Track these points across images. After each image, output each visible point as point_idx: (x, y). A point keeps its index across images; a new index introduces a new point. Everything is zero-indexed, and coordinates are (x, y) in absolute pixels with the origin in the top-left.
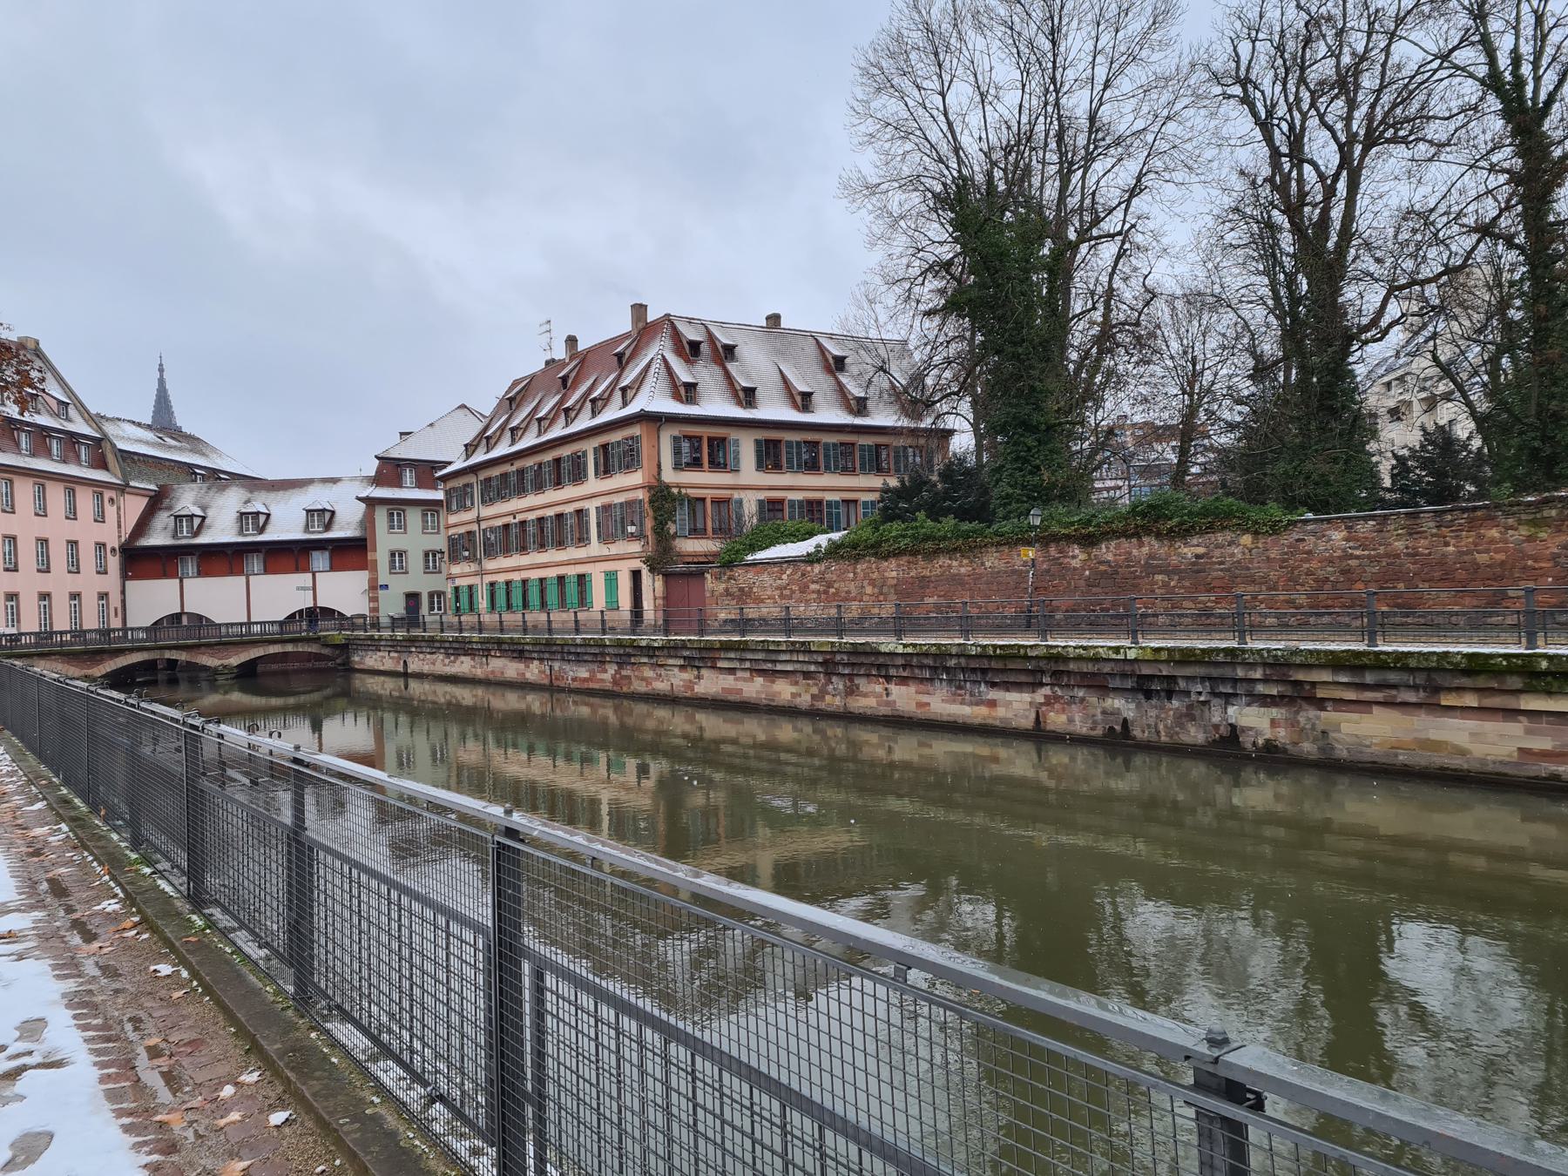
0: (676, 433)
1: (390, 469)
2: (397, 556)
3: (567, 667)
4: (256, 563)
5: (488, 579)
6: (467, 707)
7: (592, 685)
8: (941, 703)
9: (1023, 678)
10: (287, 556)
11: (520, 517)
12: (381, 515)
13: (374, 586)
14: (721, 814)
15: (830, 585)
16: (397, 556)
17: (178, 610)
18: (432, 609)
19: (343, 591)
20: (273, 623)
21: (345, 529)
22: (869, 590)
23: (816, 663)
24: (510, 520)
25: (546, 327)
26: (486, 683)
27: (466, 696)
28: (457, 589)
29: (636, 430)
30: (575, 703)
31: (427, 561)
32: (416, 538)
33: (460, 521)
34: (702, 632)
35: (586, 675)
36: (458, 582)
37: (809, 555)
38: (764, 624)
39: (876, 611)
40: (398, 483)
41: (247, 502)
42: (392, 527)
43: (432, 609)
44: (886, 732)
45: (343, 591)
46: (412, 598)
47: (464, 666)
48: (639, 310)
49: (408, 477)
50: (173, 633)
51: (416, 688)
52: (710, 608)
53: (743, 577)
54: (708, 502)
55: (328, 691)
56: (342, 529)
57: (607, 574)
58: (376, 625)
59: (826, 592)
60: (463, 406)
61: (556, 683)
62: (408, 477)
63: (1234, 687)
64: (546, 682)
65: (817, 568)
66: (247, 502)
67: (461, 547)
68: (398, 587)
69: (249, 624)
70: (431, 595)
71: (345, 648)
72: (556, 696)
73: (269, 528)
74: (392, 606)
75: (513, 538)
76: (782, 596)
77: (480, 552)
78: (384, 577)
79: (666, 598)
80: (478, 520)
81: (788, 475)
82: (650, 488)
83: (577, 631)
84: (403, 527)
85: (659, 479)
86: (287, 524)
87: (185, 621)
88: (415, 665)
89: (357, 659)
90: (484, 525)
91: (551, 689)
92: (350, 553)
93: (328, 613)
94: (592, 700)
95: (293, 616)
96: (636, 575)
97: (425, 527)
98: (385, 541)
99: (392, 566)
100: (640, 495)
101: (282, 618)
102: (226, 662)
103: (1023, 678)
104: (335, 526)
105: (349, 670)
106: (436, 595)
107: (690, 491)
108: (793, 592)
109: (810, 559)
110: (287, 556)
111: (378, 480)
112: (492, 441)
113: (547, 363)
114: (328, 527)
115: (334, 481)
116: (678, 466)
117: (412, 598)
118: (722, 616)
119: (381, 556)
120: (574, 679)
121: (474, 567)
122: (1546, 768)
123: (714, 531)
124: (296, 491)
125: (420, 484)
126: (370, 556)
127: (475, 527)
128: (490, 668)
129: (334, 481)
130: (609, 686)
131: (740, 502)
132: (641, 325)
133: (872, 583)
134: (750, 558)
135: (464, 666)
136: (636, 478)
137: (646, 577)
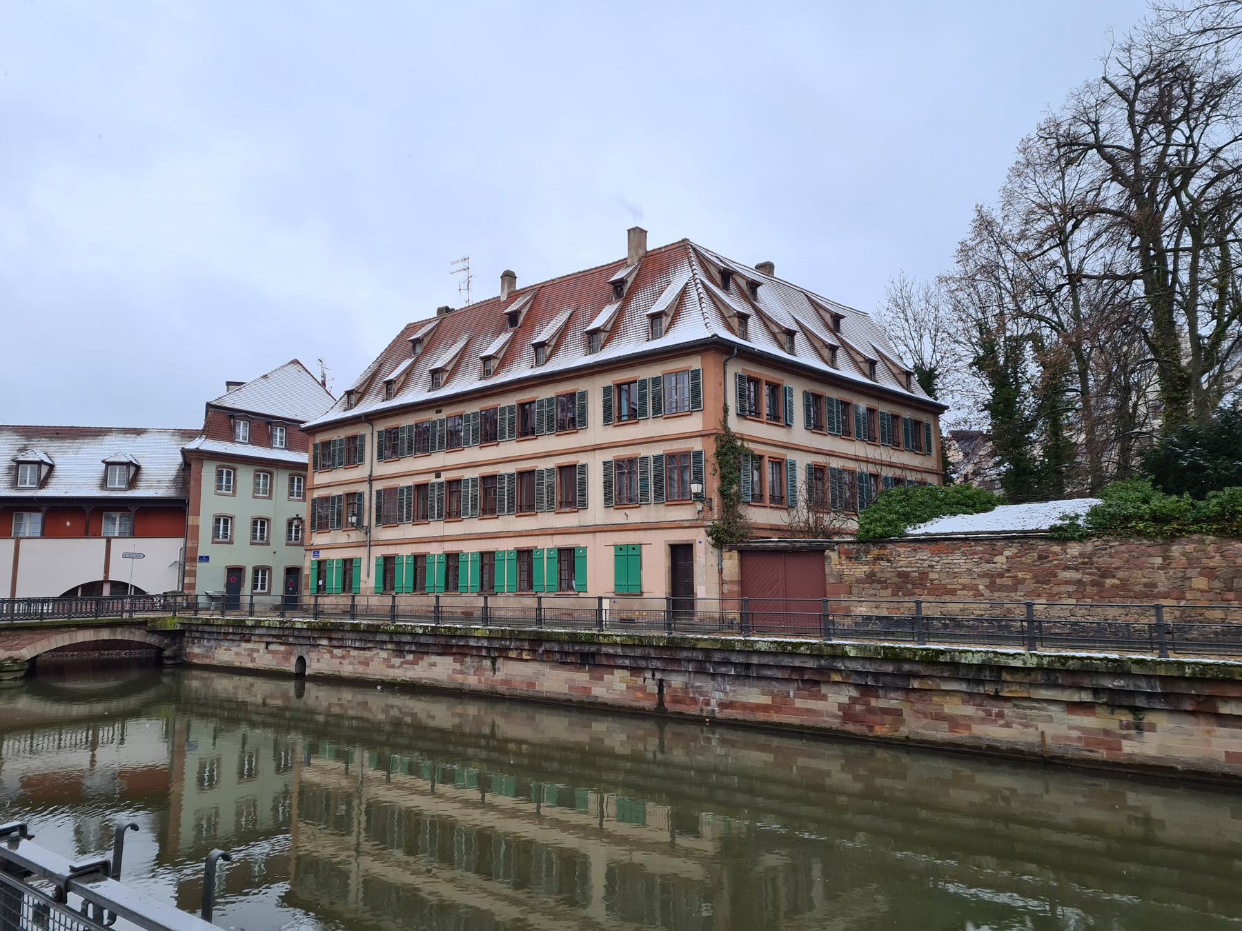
0: (740, 372)
1: (221, 419)
2: (223, 522)
3: (706, 684)
4: (31, 523)
5: (379, 552)
6: (441, 731)
7: (775, 718)
8: (556, 680)
9: (779, 674)
10: (73, 516)
11: (445, 477)
12: (208, 473)
13: (190, 558)
14: (780, 881)
15: (1106, 573)
16: (223, 522)
17: (100, 577)
18: (255, 587)
19: (149, 564)
20: (44, 601)
21: (157, 483)
22: (1200, 583)
23: (839, 671)
24: (432, 479)
25: (462, 265)
26: (490, 697)
27: (440, 715)
28: (320, 563)
29: (695, 363)
30: (723, 741)
31: (255, 530)
32: (243, 502)
33: (332, 481)
34: (827, 633)
35: (766, 700)
36: (323, 555)
37: (1054, 529)
38: (954, 627)
39: (1218, 614)
40: (231, 437)
41: (23, 450)
42: (219, 487)
43: (255, 587)
44: (482, 705)
45: (149, 564)
46: (235, 574)
47: (440, 669)
48: (637, 235)
49: (242, 430)
50: (90, 606)
51: (317, 696)
52: (837, 599)
53: (905, 559)
54: (766, 459)
55: (150, 694)
56: (150, 487)
57: (619, 548)
58: (193, 606)
59: (1100, 585)
60: (296, 362)
61: (670, 707)
62: (242, 430)
63: (877, 681)
64: (650, 704)
65: (1074, 549)
66: (23, 450)
67: (329, 514)
68: (220, 558)
69: (12, 601)
70: (256, 571)
71: (177, 635)
72: (670, 729)
73: (53, 482)
74: (210, 582)
75: (490, 496)
76: (992, 587)
77: (369, 517)
78: (205, 545)
79: (743, 582)
80: (371, 480)
81: (829, 438)
82: (718, 437)
83: (353, 617)
84: (232, 488)
85: (725, 427)
86: (77, 475)
87: (106, 591)
88: (321, 661)
89: (197, 650)
90: (378, 486)
91: (660, 716)
92: (165, 515)
93: (120, 588)
94: (776, 742)
95: (73, 591)
96: (681, 555)
97: (256, 490)
98: (211, 501)
99: (216, 534)
100: (697, 445)
101: (57, 595)
102: (15, 654)
103: (779, 674)
104: (141, 484)
105: (184, 665)
106: (262, 571)
107: (752, 446)
108: (1018, 582)
109: (1059, 535)
110: (73, 516)
111: (209, 431)
112: (395, 387)
113: (440, 311)
114: (132, 483)
115: (138, 432)
116: (741, 415)
117: (235, 574)
118: (862, 610)
119: (204, 522)
120: (723, 705)
121: (356, 536)
122: (761, 717)
123: (773, 499)
124: (87, 440)
125: (253, 441)
126: (191, 520)
127: (363, 488)
128: (500, 675)
129: (138, 432)
130: (835, 723)
131: (793, 465)
132: (641, 253)
133: (1209, 573)
134: (910, 530)
135: (440, 669)
136: (695, 423)
137: (705, 559)
